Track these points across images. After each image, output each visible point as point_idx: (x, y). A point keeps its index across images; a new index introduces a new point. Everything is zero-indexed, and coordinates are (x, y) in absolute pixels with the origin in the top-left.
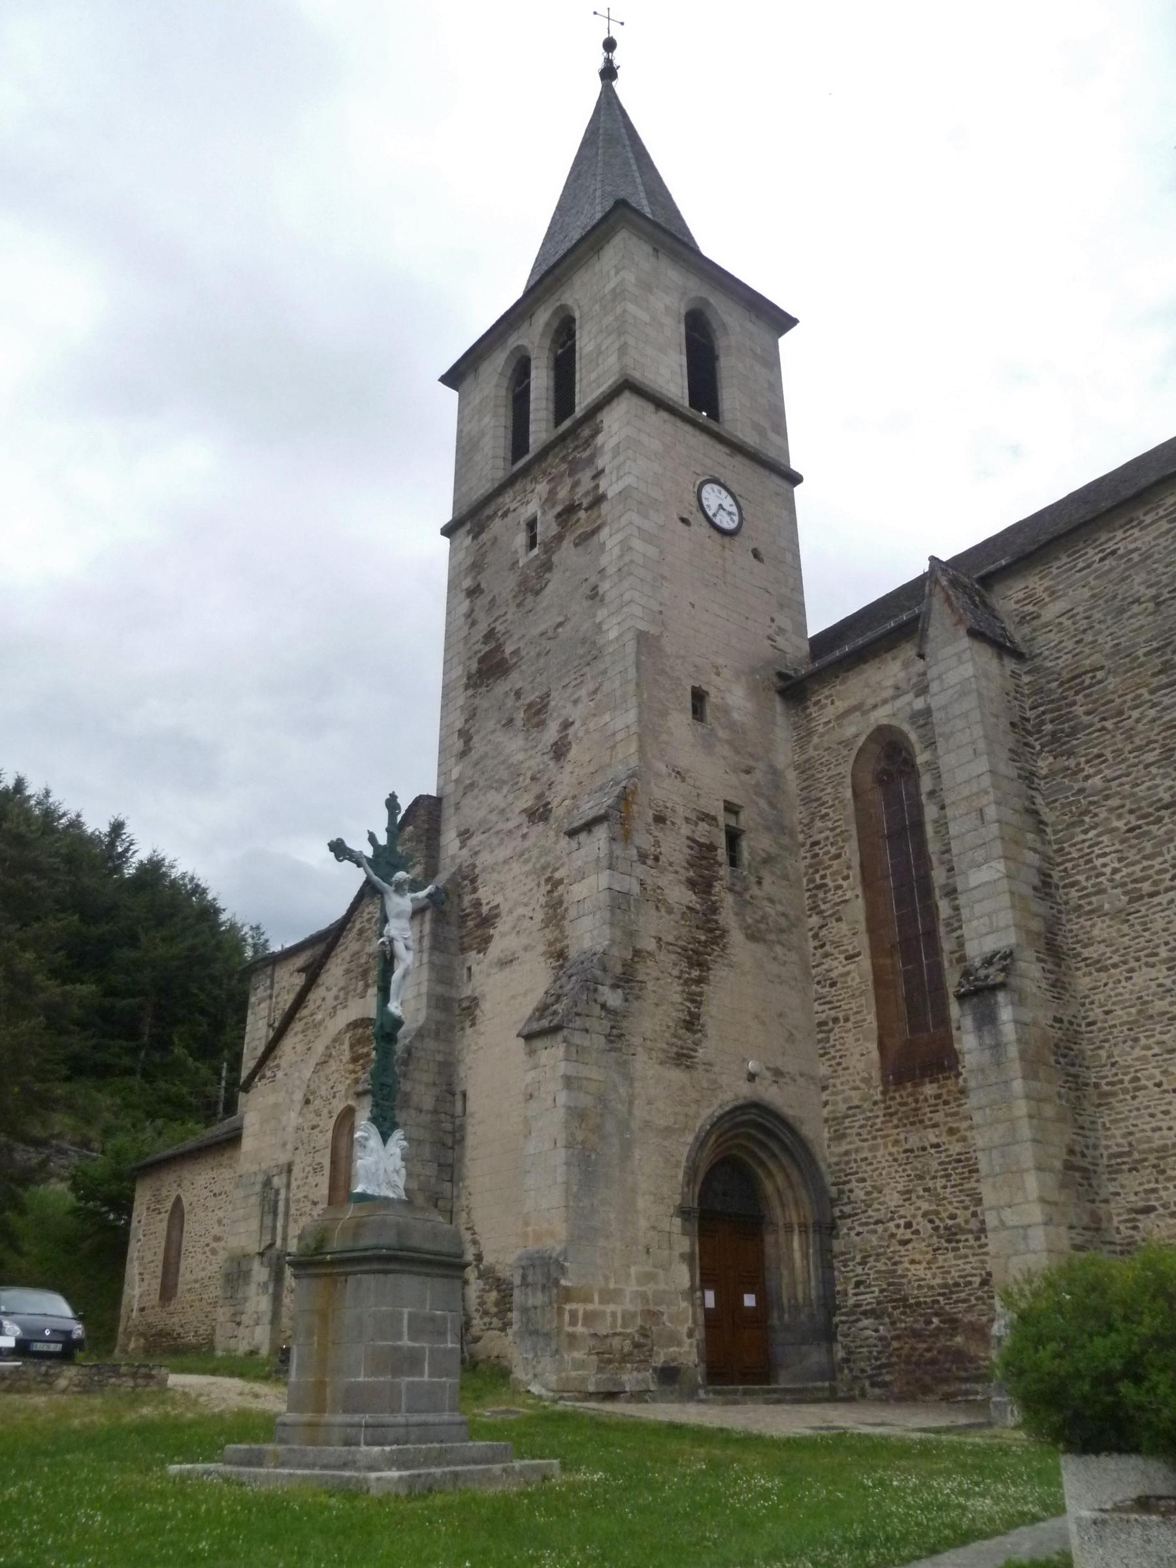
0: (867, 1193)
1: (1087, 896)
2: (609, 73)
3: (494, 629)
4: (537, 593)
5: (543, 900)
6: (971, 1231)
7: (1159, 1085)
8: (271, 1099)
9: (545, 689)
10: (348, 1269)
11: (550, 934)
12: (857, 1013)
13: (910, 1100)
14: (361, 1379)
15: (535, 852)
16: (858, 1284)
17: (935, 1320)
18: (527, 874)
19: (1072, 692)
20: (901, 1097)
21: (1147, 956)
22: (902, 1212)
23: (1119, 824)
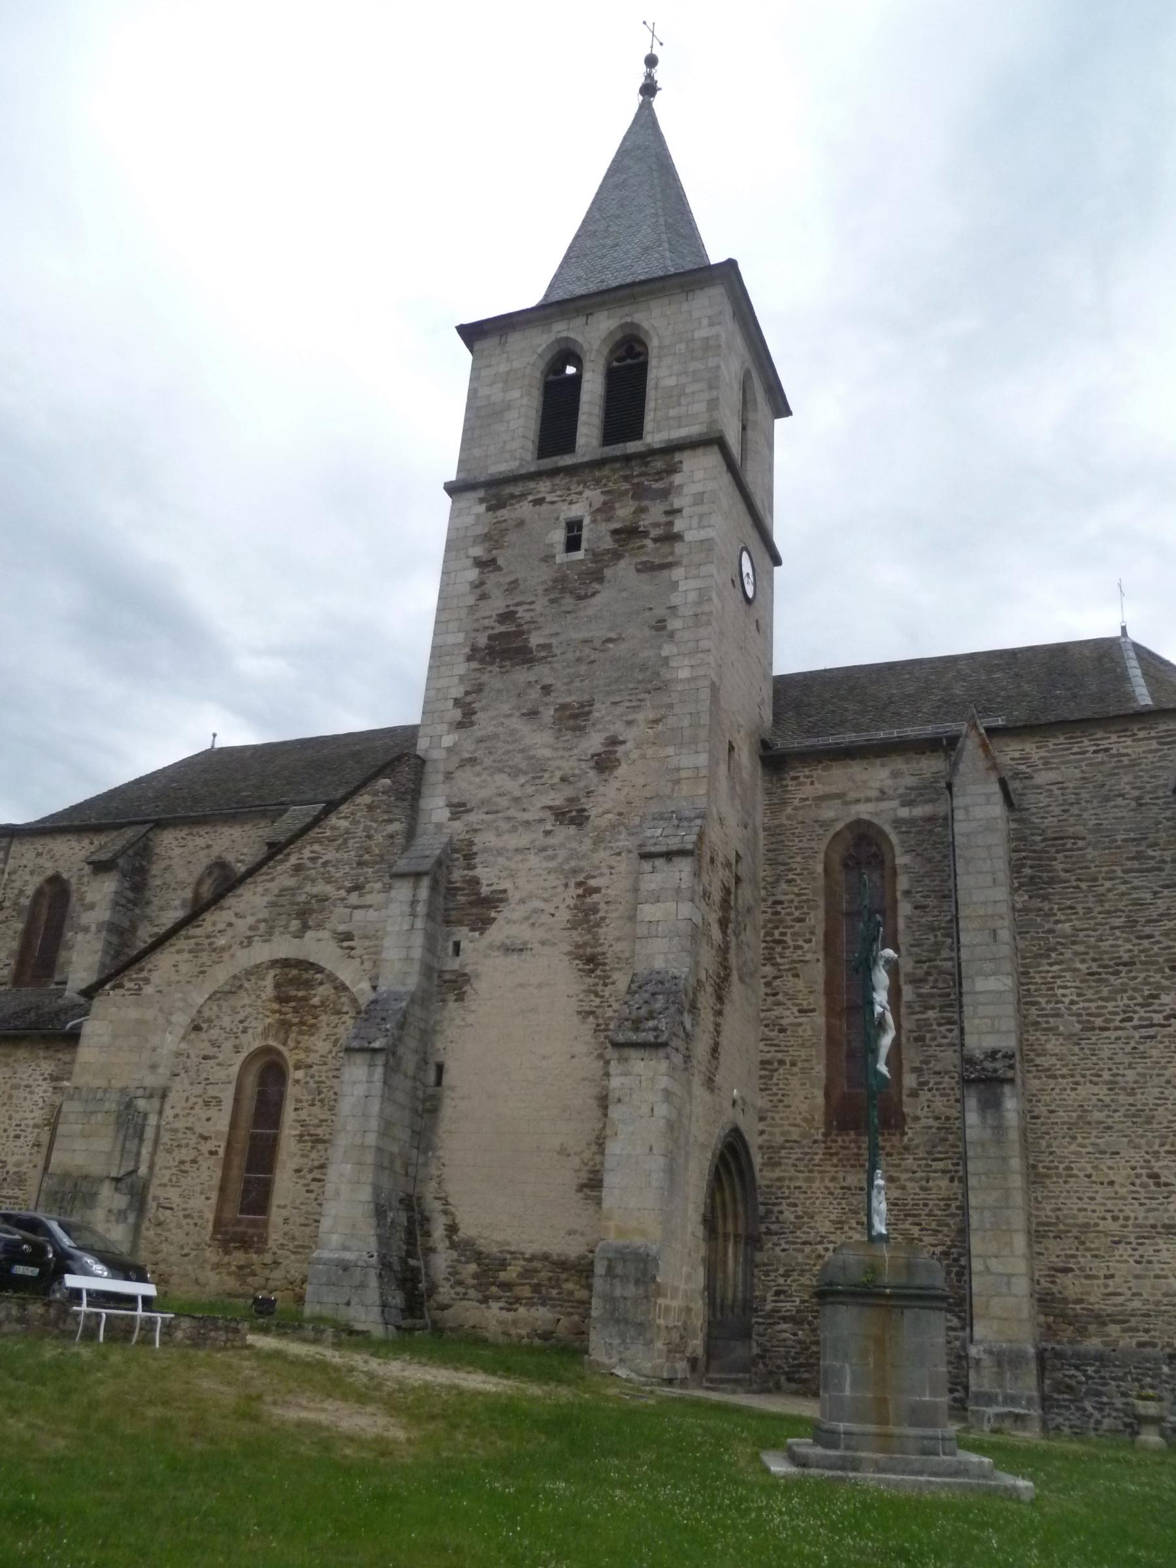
0: (797, 1217)
1: (1046, 1016)
2: (649, 89)
3: (515, 613)
5: (571, 902)
7: (1089, 1176)
8: (134, 1014)
9: (586, 697)
10: (905, 1303)
11: (577, 936)
12: (806, 1061)
14: (927, 1398)
15: (562, 854)
16: (778, 1293)
19: (1053, 850)
20: (843, 1141)
21: (1092, 1075)
22: (832, 1237)
23: (1083, 967)
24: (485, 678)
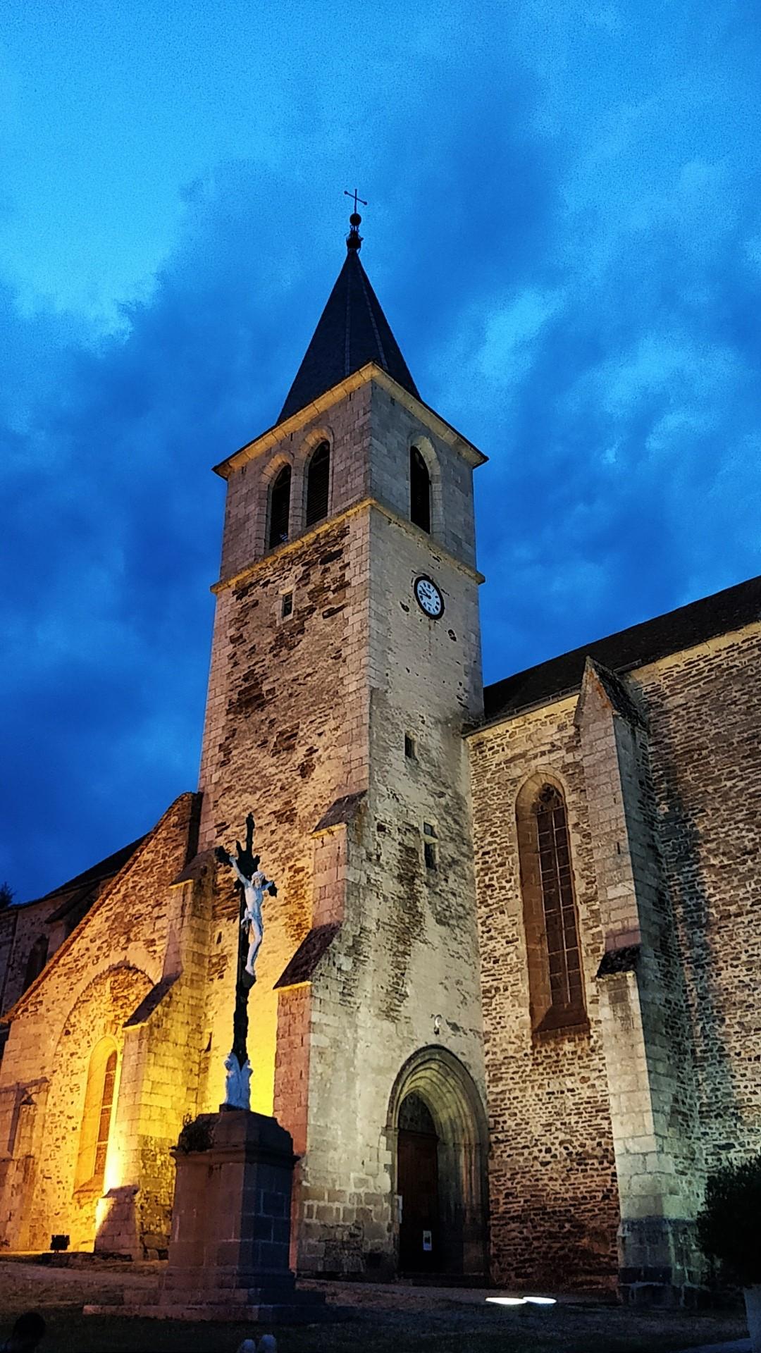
2: (354, 242)
4: (291, 649)
6: (596, 1157)
7: (739, 1054)
13: (553, 1054)
15: (282, 844)
16: (507, 1195)
17: (567, 1225)
18: (274, 861)
22: (543, 1140)
24: (236, 725)
